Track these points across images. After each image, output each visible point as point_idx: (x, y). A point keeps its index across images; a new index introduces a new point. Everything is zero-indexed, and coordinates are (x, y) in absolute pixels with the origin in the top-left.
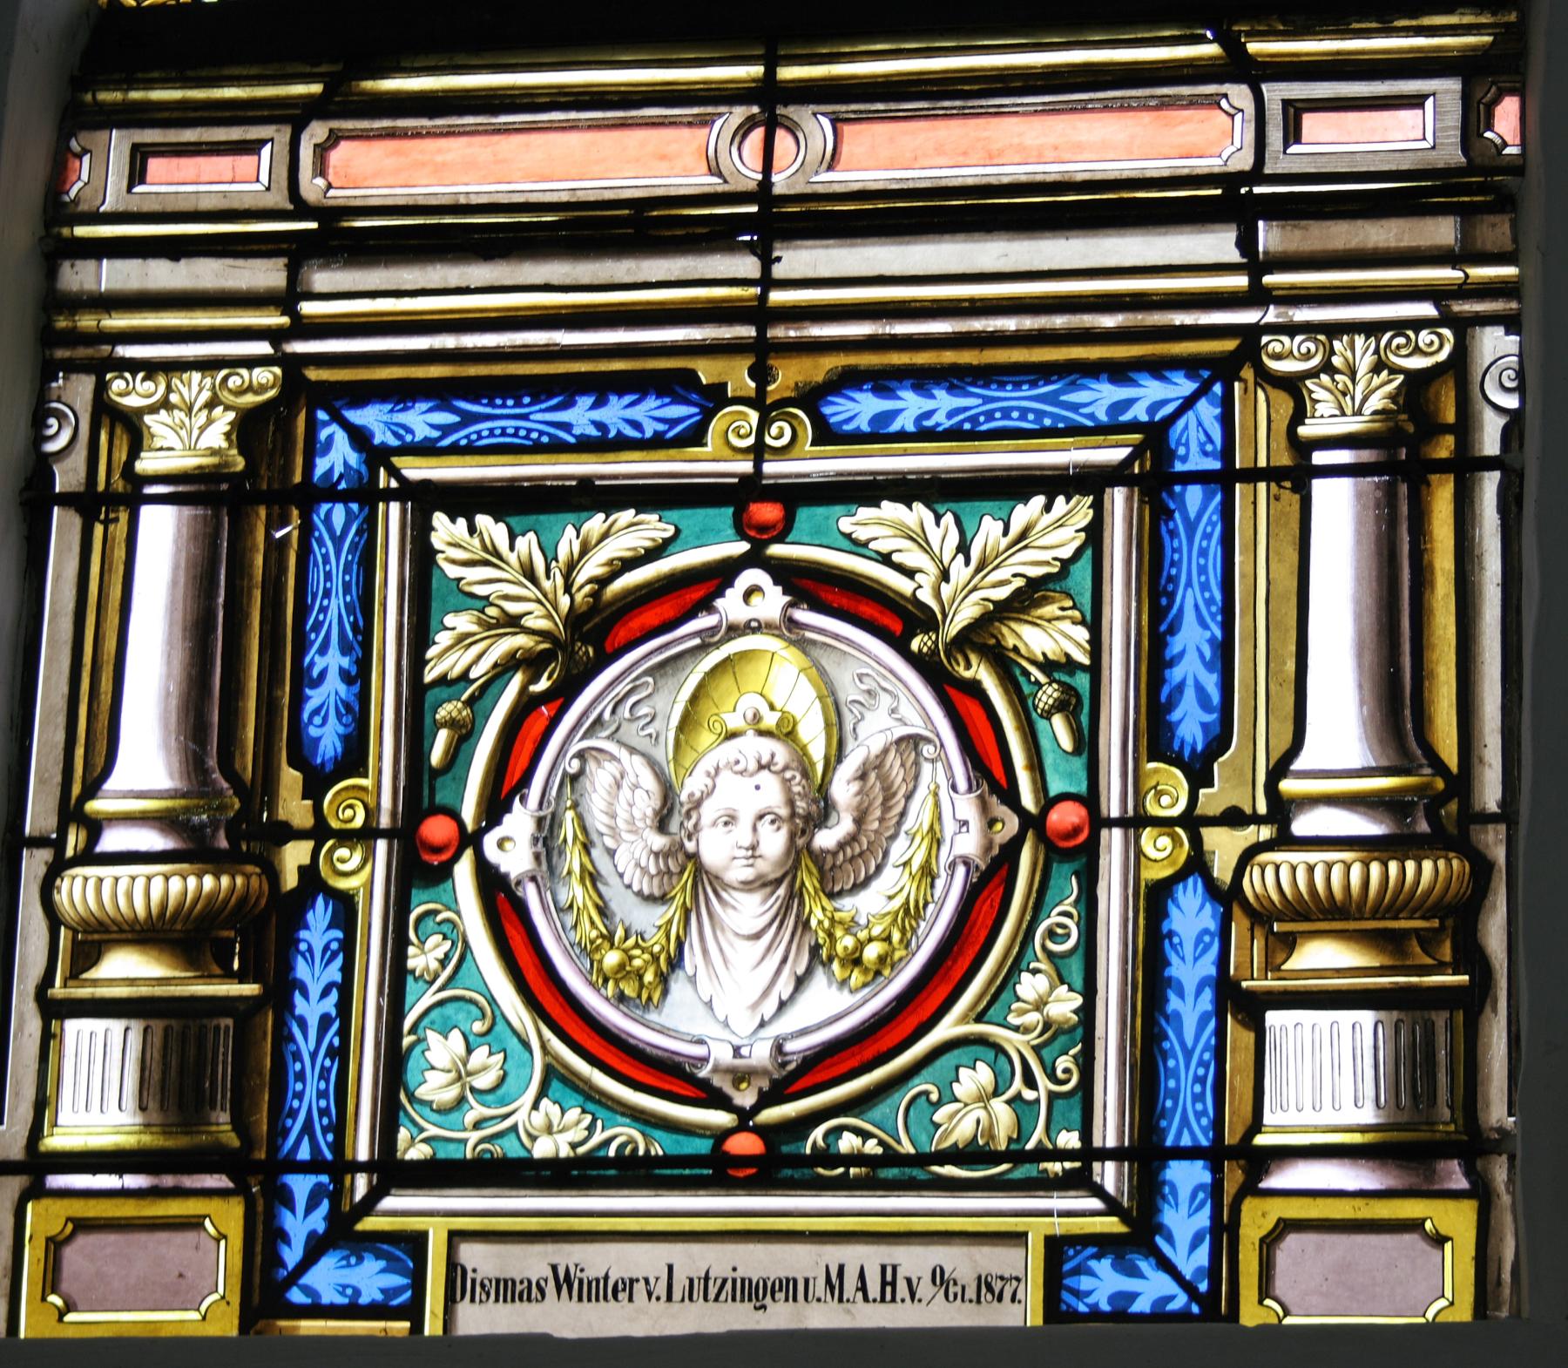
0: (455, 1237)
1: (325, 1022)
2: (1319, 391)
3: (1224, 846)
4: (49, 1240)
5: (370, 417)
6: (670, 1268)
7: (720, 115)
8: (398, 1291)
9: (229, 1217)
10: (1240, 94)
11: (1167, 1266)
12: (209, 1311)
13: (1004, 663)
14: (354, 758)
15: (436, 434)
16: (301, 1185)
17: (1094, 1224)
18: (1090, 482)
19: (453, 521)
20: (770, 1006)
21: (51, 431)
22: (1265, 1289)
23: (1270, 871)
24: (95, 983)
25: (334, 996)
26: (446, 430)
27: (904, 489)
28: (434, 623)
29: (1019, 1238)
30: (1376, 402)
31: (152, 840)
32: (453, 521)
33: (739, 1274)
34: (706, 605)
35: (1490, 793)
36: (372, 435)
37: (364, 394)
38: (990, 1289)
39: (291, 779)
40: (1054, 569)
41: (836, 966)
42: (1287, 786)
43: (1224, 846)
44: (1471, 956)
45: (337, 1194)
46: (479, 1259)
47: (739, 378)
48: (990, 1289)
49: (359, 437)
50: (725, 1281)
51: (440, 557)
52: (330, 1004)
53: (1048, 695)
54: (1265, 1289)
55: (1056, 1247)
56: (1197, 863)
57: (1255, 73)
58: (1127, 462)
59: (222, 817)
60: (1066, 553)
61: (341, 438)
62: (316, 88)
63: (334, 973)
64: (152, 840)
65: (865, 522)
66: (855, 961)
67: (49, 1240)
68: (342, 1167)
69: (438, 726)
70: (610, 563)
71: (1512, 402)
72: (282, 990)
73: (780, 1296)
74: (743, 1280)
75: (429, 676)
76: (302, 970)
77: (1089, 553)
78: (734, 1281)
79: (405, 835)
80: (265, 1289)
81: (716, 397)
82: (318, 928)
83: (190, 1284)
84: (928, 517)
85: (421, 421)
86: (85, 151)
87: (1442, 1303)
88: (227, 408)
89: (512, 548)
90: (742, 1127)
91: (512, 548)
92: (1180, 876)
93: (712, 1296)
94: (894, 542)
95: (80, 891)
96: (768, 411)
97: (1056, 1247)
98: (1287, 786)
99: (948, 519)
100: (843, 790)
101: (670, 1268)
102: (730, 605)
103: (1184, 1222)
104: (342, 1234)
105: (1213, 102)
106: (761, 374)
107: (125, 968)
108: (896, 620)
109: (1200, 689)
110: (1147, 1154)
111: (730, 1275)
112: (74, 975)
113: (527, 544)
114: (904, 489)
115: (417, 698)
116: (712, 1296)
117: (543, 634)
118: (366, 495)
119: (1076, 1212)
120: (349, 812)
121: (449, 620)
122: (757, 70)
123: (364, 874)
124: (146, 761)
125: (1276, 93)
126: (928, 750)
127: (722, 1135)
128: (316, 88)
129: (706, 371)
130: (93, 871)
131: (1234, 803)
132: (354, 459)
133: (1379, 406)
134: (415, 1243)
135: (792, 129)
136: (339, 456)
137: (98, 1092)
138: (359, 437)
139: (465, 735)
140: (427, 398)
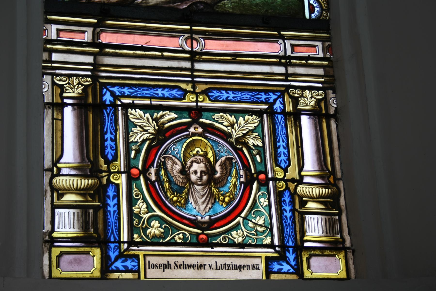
0: (145, 255)
2: (302, 100)
3: (292, 186)
4: (57, 256)
5: (115, 89)
7: (182, 36)
8: (135, 266)
9: (97, 252)
10: (281, 41)
12: (95, 271)
13: (246, 145)
14: (115, 157)
15: (129, 94)
16: (112, 245)
18: (259, 113)
19: (132, 110)
21: (44, 87)
22: (309, 267)
23: (301, 188)
25: (116, 206)
26: (132, 93)
28: (129, 131)
30: (312, 104)
32: (132, 110)
34: (186, 130)
35: (339, 175)
37: (114, 85)
38: (254, 267)
39: (102, 161)
41: (220, 202)
42: (303, 173)
44: (338, 208)
45: (120, 248)
46: (153, 260)
48: (254, 267)
49: (113, 94)
50: (230, 265)
51: (129, 117)
52: (115, 208)
53: (255, 152)
54: (309, 267)
55: (267, 258)
56: (287, 188)
57: (283, 38)
58: (267, 109)
60: (256, 125)
62: (96, 21)
63: (115, 201)
66: (223, 201)
67: (57, 256)
68: (120, 242)
69: (132, 150)
71: (335, 106)
72: (105, 205)
74: (235, 265)
76: (109, 201)
77: (260, 126)
78: (232, 265)
79: (128, 172)
81: (186, 92)
82: (111, 192)
85: (126, 91)
86: (47, 29)
87: (340, 271)
89: (144, 116)
90: (203, 233)
91: (144, 116)
93: (227, 268)
94: (223, 121)
95: (59, 181)
96: (197, 94)
97: (267, 258)
98: (303, 173)
102: (192, 130)
103: (291, 257)
104: (121, 256)
105: (277, 42)
106: (194, 87)
107: (69, 198)
108: (226, 136)
109: (284, 153)
110: (283, 246)
111: (231, 264)
112: (58, 199)
113: (148, 115)
115: (128, 145)
116: (227, 268)
117: (152, 134)
118: (114, 106)
119: (271, 253)
122: (189, 27)
124: (70, 154)
126: (234, 161)
128: (96, 21)
129: (183, 86)
130: (61, 178)
131: (293, 177)
132: (112, 99)
134: (137, 257)
135: (196, 40)
136: (108, 98)
137: (66, 224)
139: (138, 152)
140: (127, 86)
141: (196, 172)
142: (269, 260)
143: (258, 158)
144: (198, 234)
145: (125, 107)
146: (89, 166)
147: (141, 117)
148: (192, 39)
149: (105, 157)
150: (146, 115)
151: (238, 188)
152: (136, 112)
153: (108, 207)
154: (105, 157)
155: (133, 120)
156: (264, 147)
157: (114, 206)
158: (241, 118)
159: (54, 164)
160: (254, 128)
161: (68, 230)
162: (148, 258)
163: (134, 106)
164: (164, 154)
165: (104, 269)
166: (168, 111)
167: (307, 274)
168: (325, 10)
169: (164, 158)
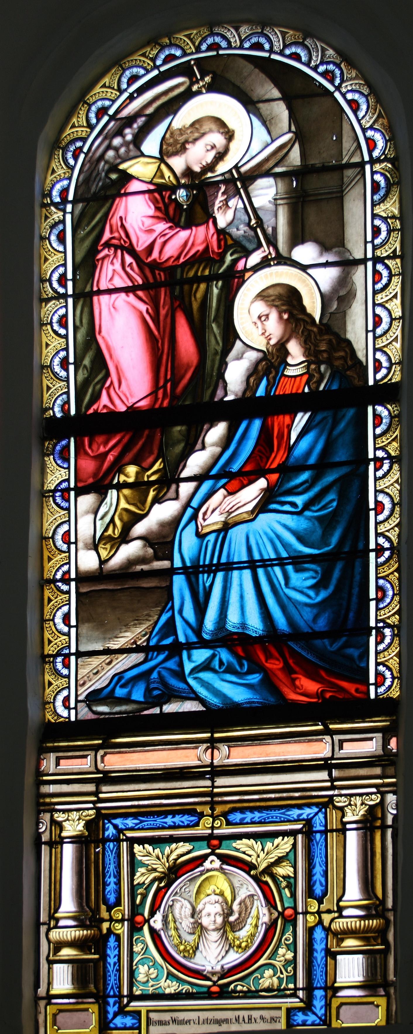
0: (148, 1012)
5: (118, 821)
9: (94, 1009)
10: (328, 738)
13: (274, 877)
18: (293, 833)
22: (338, 1018)
24: (60, 956)
25: (117, 958)
26: (137, 824)
27: (248, 836)
29: (280, 1008)
37: (116, 816)
39: (103, 908)
42: (341, 904)
44: (385, 942)
47: (207, 810)
48: (273, 1020)
49: (116, 827)
52: (116, 959)
53: (284, 884)
55: (289, 1010)
56: (320, 922)
57: (331, 733)
60: (288, 850)
61: (111, 827)
62: (100, 742)
63: (116, 952)
73: (225, 1023)
76: (109, 952)
77: (293, 850)
79: (131, 920)
82: (112, 942)
85: (130, 822)
94: (246, 848)
95: (55, 935)
97: (289, 1010)
98: (341, 904)
99: (259, 843)
100: (236, 907)
102: (207, 865)
103: (318, 1004)
104: (122, 1011)
105: (321, 740)
107: (67, 952)
110: (309, 988)
113: (157, 851)
114: (248, 836)
115: (133, 889)
117: (162, 873)
118: (117, 840)
119: (293, 1002)
122: (209, 735)
123: (122, 929)
124: (68, 904)
128: (100, 742)
132: (114, 832)
134: (139, 1013)
137: (62, 980)
138: (116, 827)
139: (144, 897)
141: (209, 915)
142: (290, 1012)
143: (287, 892)
144: (209, 987)
145: (132, 841)
146: (87, 916)
147: (150, 853)
148: (213, 748)
149: (106, 902)
150: (155, 850)
151: (259, 928)
152: (144, 848)
153: (108, 958)
154: (106, 902)
155: (139, 858)
156: (295, 878)
157: (115, 957)
158: (268, 843)
159: (51, 917)
160: (285, 854)
161: (62, 986)
162: (152, 1015)
163: (141, 841)
164: (174, 896)
165: (102, 1026)
166: (182, 843)
167: (335, 1024)
168: (396, 594)
169: (173, 901)
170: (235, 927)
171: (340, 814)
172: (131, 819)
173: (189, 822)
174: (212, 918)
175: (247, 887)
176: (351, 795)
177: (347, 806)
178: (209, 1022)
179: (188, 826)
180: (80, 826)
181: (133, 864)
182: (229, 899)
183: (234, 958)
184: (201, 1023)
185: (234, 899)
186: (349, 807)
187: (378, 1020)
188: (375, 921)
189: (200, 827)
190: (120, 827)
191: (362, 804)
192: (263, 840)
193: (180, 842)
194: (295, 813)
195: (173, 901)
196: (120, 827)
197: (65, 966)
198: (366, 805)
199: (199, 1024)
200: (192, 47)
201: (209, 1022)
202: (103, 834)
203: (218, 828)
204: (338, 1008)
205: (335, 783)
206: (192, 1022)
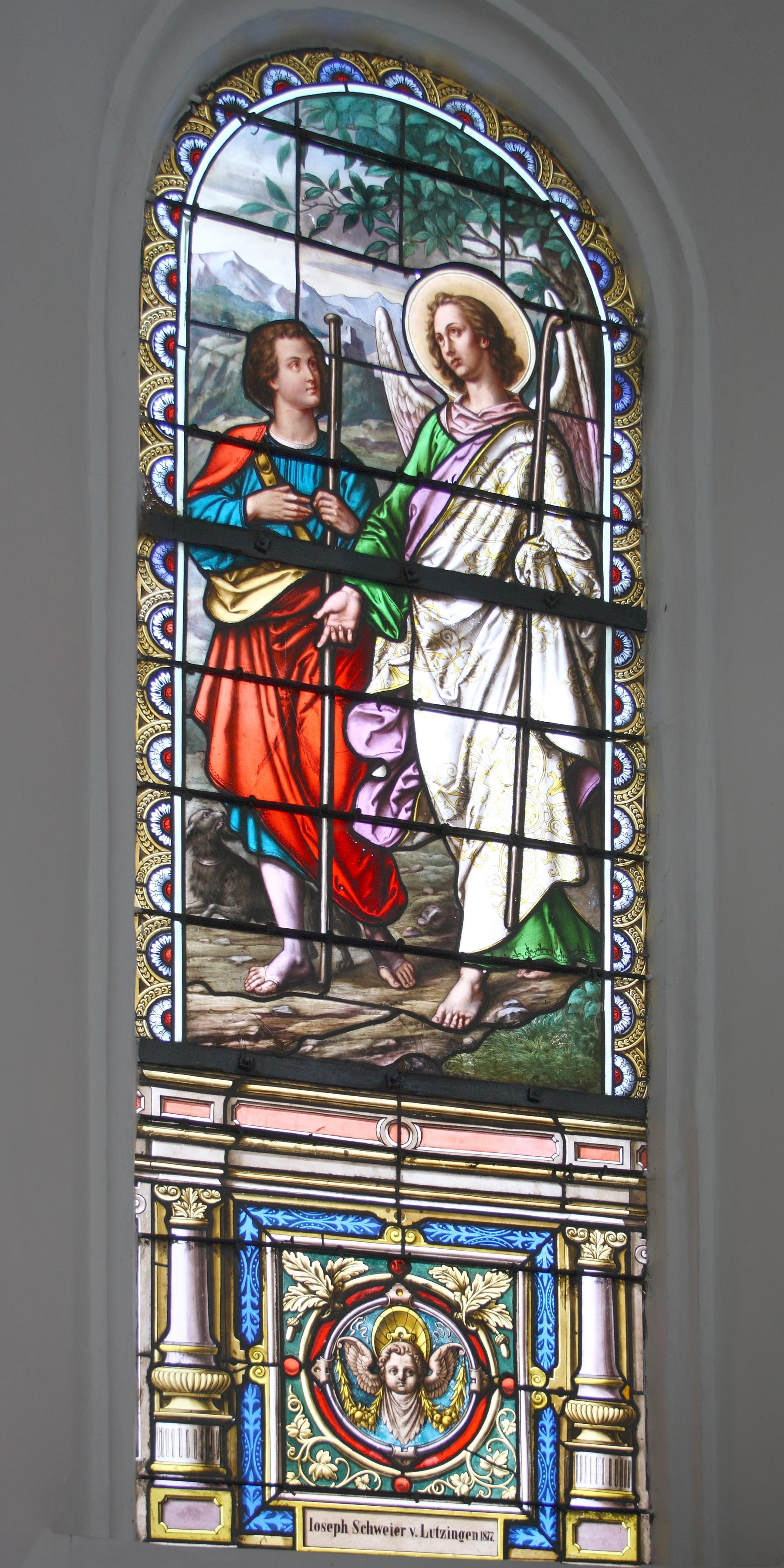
0: (304, 1509)
1: (256, 1432)
3: (557, 1401)
5: (261, 1214)
6: (423, 1526)
8: (287, 1526)
9: (225, 1499)
10: (557, 1136)
11: (542, 1532)
13: (484, 1324)
14: (259, 1338)
16: (251, 1489)
17: (142, 1293)
18: (511, 1269)
20: (412, 1437)
22: (575, 1540)
24: (169, 1410)
25: (259, 1423)
26: (291, 1222)
27: (451, 1262)
29: (496, 1520)
31: (187, 1360)
33: (451, 1530)
34: (382, 1294)
35: (639, 1385)
36: (262, 1221)
37: (259, 1206)
39: (236, 1342)
40: (499, 1295)
43: (557, 1401)
45: (263, 1493)
46: (319, 1517)
47: (390, 1216)
49: (257, 1222)
53: (499, 1338)
56: (550, 1404)
57: (561, 1129)
59: (214, 1354)
60: (503, 1290)
61: (249, 1221)
64: (187, 1360)
65: (436, 1271)
66: (440, 1422)
67: (159, 1503)
69: (288, 1326)
70: (552, 1527)
71: (644, 1261)
73: (470, 1538)
75: (285, 1309)
79: (280, 1364)
80: (240, 1524)
81: (384, 1224)
82: (250, 1398)
83: (214, 1521)
84: (458, 1273)
85: (281, 1218)
88: (204, 1203)
90: (402, 1476)
92: (545, 1408)
94: (445, 1281)
96: (404, 1229)
99: (465, 1273)
100: (434, 1364)
101: (423, 1526)
102: (392, 1294)
105: (550, 1137)
107: (181, 1405)
113: (316, 1264)
114: (451, 1262)
115: (281, 1315)
117: (324, 1299)
120: (256, 1356)
121: (290, 1289)
123: (269, 1379)
124: (183, 1329)
125: (571, 1140)
127: (394, 1478)
129: (381, 1213)
133: (605, 1258)
134: (292, 1510)
137: (176, 1450)
138: (257, 1222)
139: (298, 1329)
145: (279, 1247)
147: (305, 1267)
155: (290, 1272)
156: (514, 1331)
163: (293, 1247)
169: (343, 1342)
170: (435, 1390)
171: (164, 1212)
172: (266, 1211)
173: (286, 1223)
174: (400, 1374)
175: (448, 1334)
176: (182, 1186)
177: (176, 1201)
178: (440, 1535)
179: (365, 1236)
180: (605, 1253)
181: (282, 1279)
182: (424, 1349)
183: (436, 1437)
184: (425, 1535)
185: (431, 1351)
186: (179, 1202)
187: (627, 1548)
188: (215, 1376)
189: (385, 1240)
190: (264, 1224)
191: (199, 1200)
192: (473, 1270)
193: (349, 1256)
194: (519, 1239)
195: (343, 1342)
196: (264, 1224)
197: (184, 1427)
198: (204, 1203)
199: (422, 1536)
200: (622, 365)
201: (440, 1535)
202: (237, 1230)
203: (411, 1244)
204: (163, 1504)
205: (393, 1190)
206: (407, 1532)
